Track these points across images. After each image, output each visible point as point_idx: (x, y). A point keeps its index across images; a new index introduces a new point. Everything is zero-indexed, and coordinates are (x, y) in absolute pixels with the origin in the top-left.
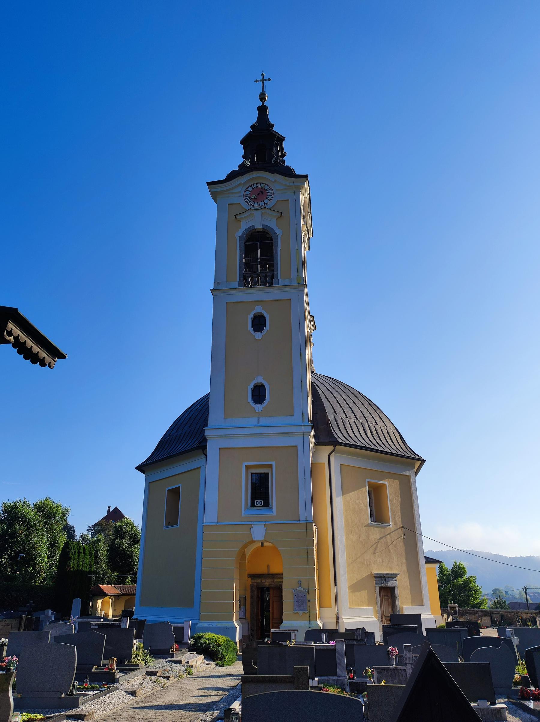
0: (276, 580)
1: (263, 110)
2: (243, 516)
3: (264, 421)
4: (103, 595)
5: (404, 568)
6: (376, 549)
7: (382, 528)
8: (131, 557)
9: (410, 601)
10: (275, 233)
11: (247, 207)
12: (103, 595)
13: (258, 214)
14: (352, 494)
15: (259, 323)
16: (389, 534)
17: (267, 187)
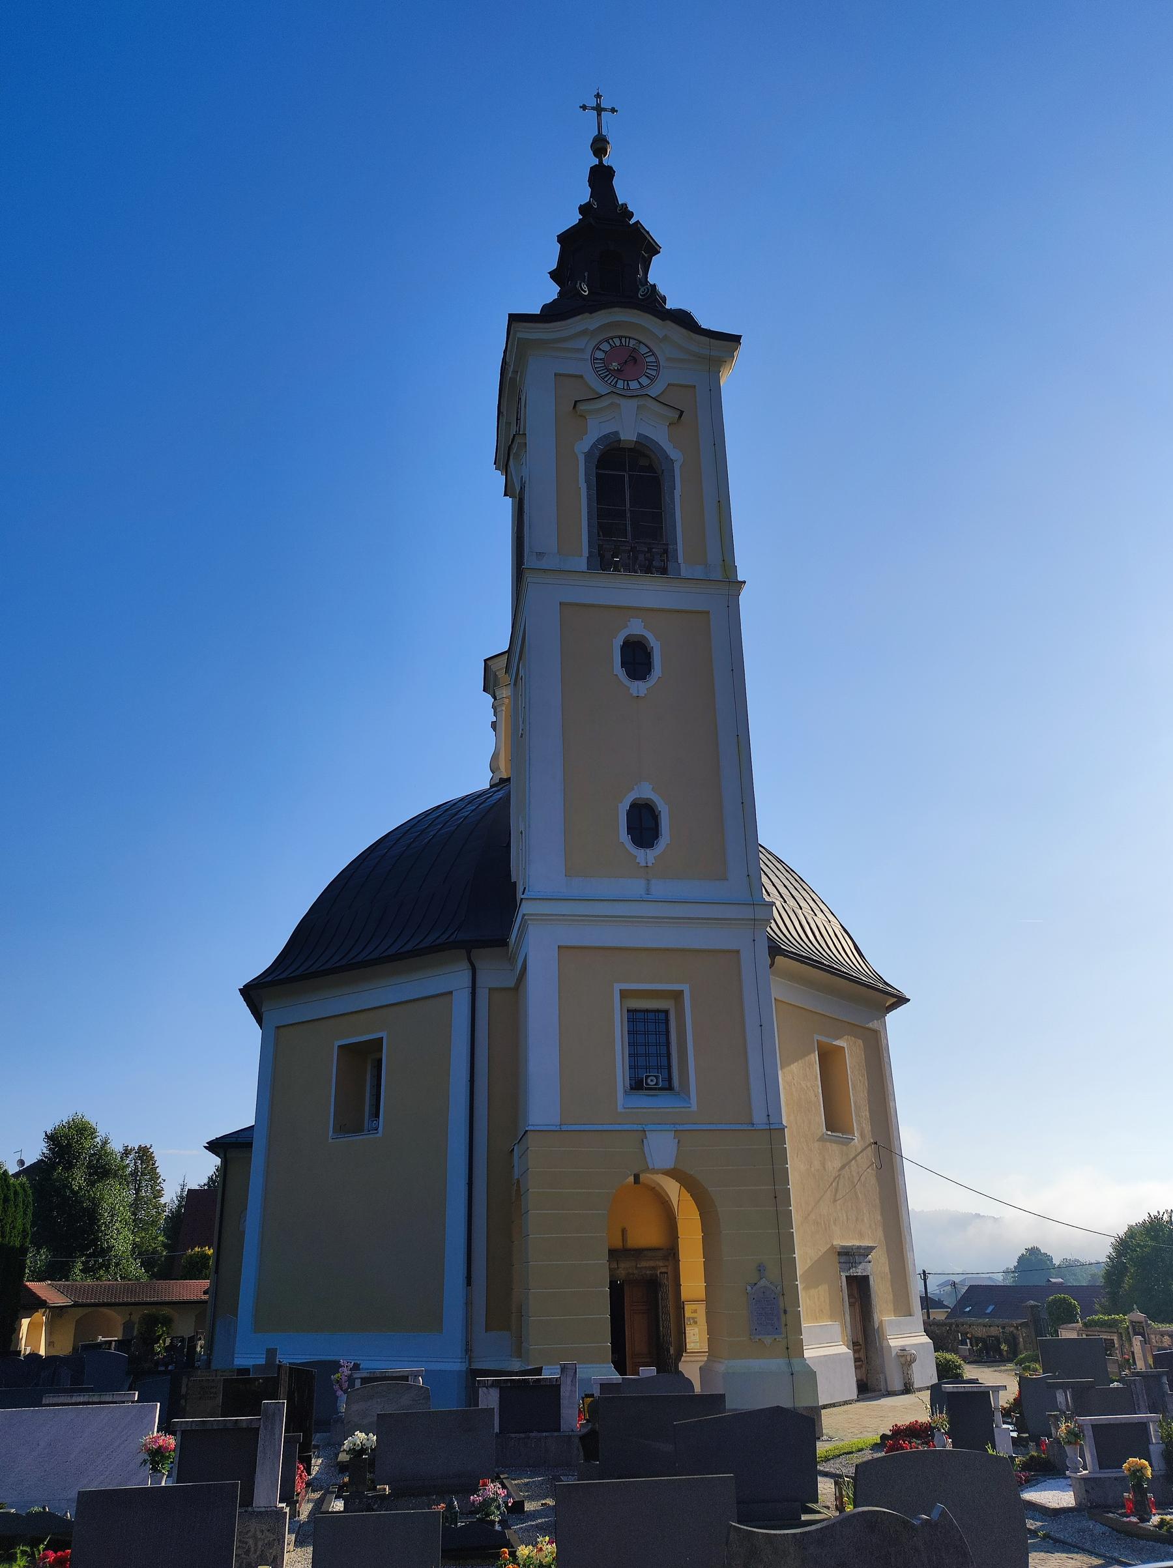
0: (644, 1264)
1: (601, 178)
2: (620, 1109)
3: (660, 888)
4: (35, 1304)
5: (880, 1233)
6: (837, 1190)
7: (843, 1144)
8: (91, 1215)
9: (891, 1306)
10: (667, 457)
11: (602, 388)
12: (35, 1304)
13: (629, 407)
14: (794, 1067)
15: (637, 659)
16: (854, 1158)
17: (643, 350)
